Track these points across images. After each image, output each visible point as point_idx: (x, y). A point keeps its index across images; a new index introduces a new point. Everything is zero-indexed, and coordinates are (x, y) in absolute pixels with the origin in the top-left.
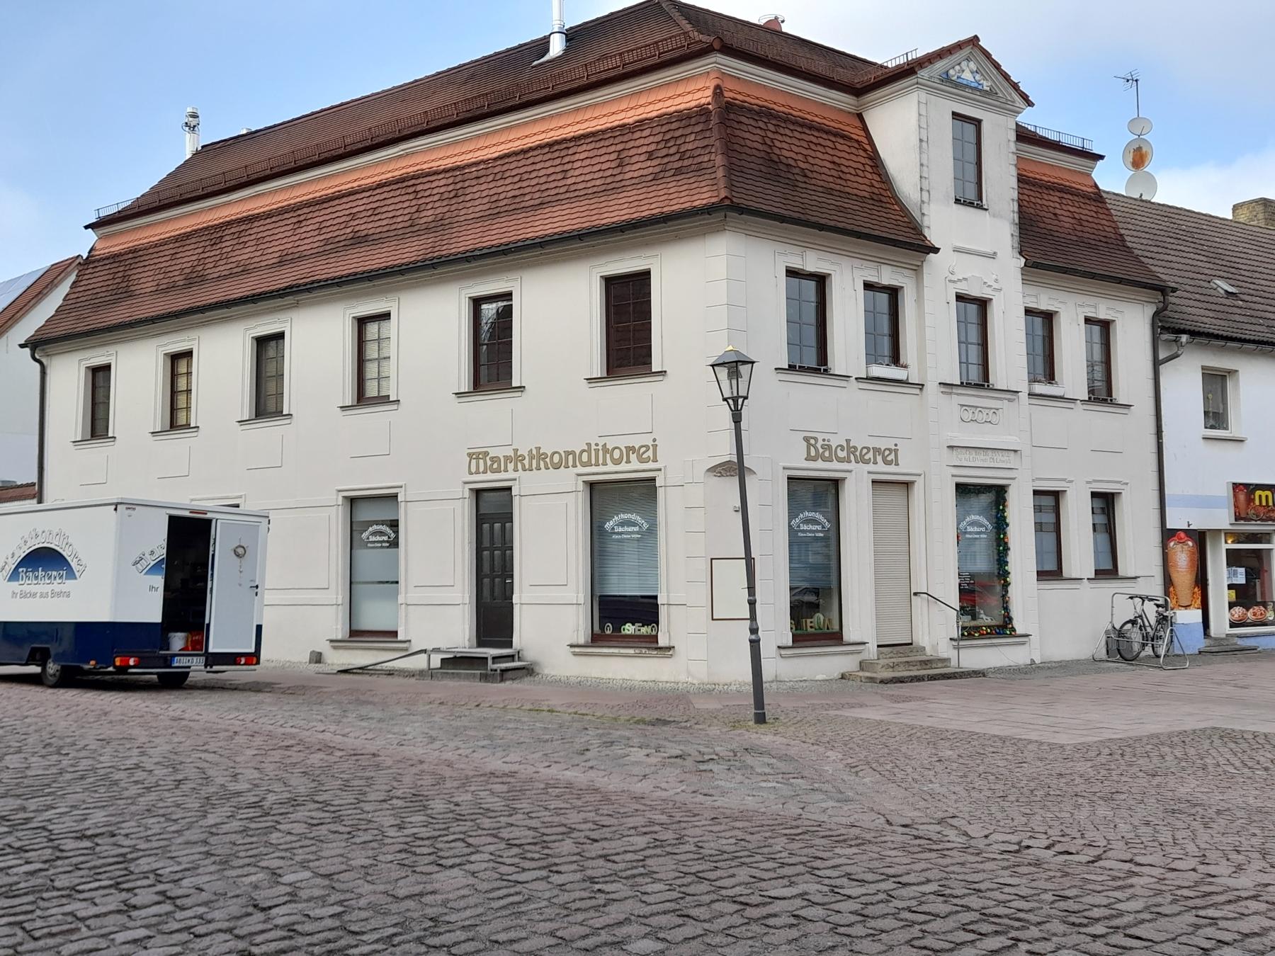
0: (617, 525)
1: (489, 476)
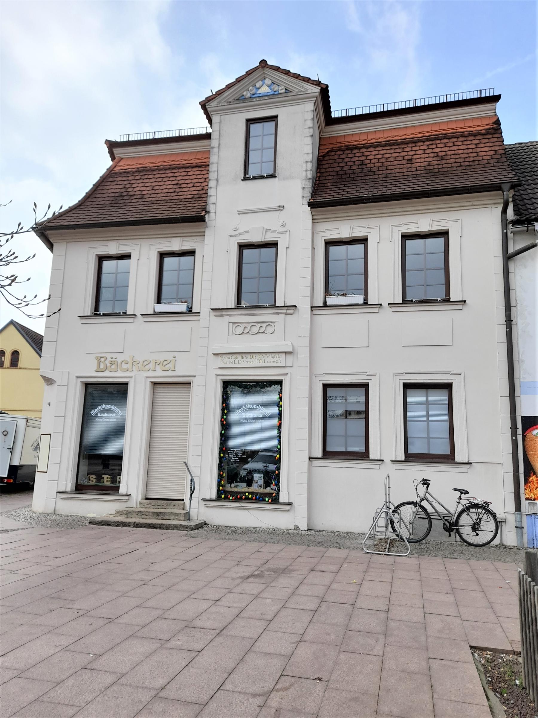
0: (244, 412)
1: (107, 373)
